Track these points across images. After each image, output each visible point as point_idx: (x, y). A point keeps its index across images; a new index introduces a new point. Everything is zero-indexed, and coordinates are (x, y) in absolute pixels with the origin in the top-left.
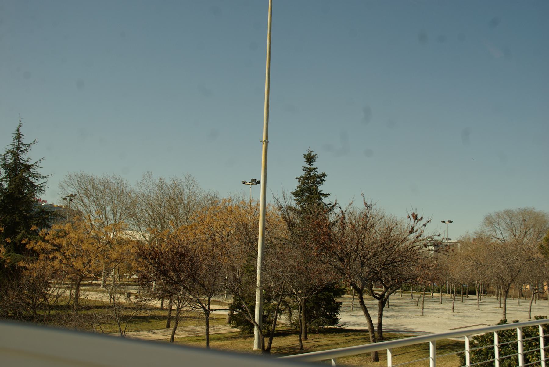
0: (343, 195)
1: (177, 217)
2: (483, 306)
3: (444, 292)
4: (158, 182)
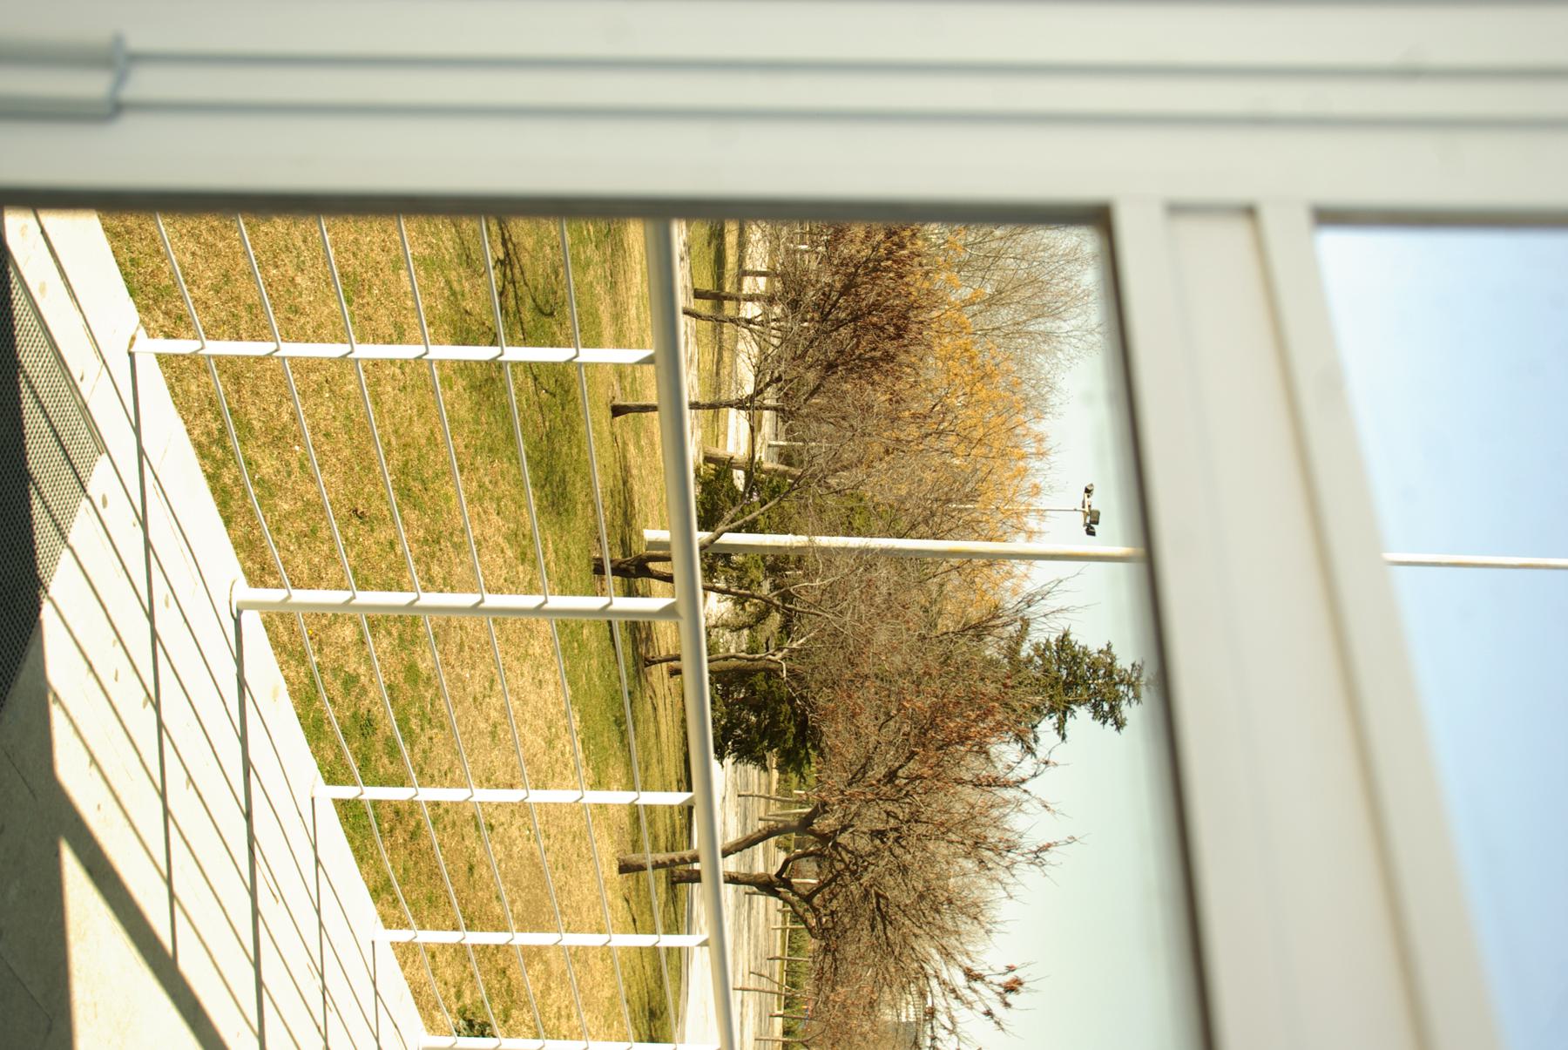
1: (993, 301)
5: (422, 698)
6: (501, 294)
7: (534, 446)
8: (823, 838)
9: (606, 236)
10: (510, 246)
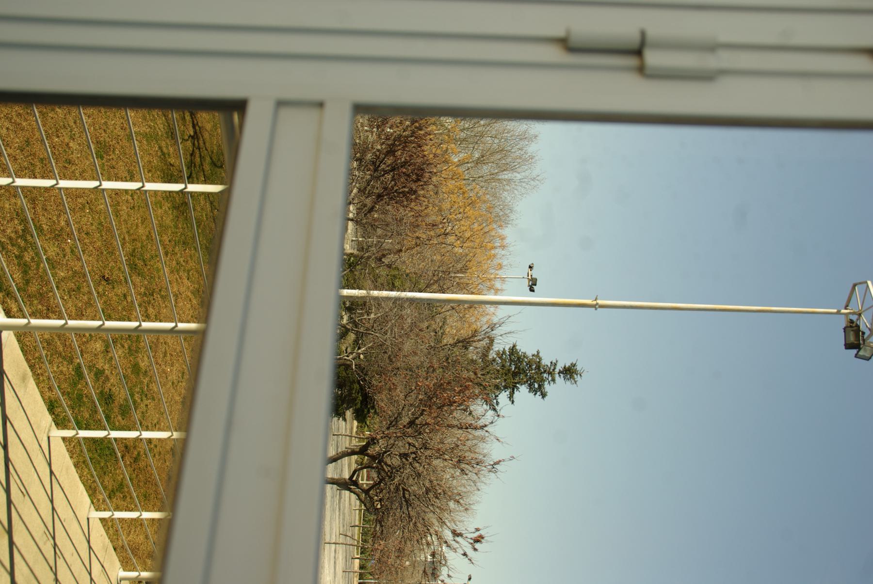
0: (511, 423)
1: (479, 162)
3: (361, 576)
5: (141, 382)
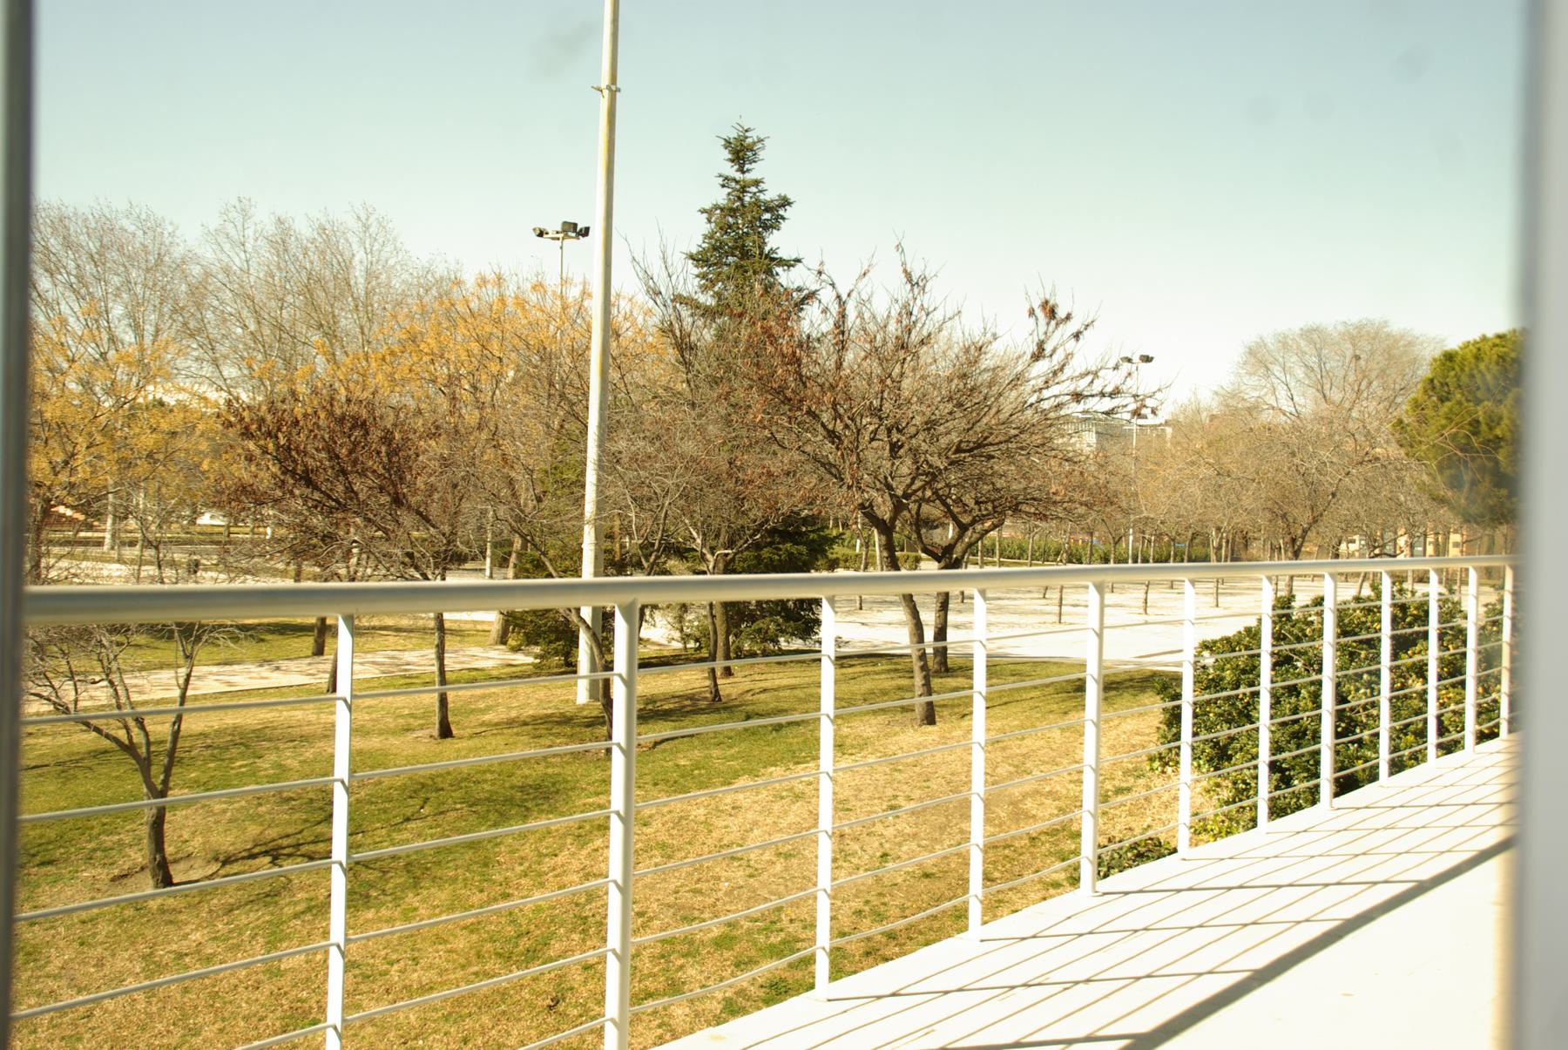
0: (840, 260)
1: (331, 334)
2: (1229, 598)
4: (270, 229)
5: (749, 932)
6: (311, 858)
7: (483, 818)
8: (898, 507)
9: (247, 747)
10: (256, 850)
